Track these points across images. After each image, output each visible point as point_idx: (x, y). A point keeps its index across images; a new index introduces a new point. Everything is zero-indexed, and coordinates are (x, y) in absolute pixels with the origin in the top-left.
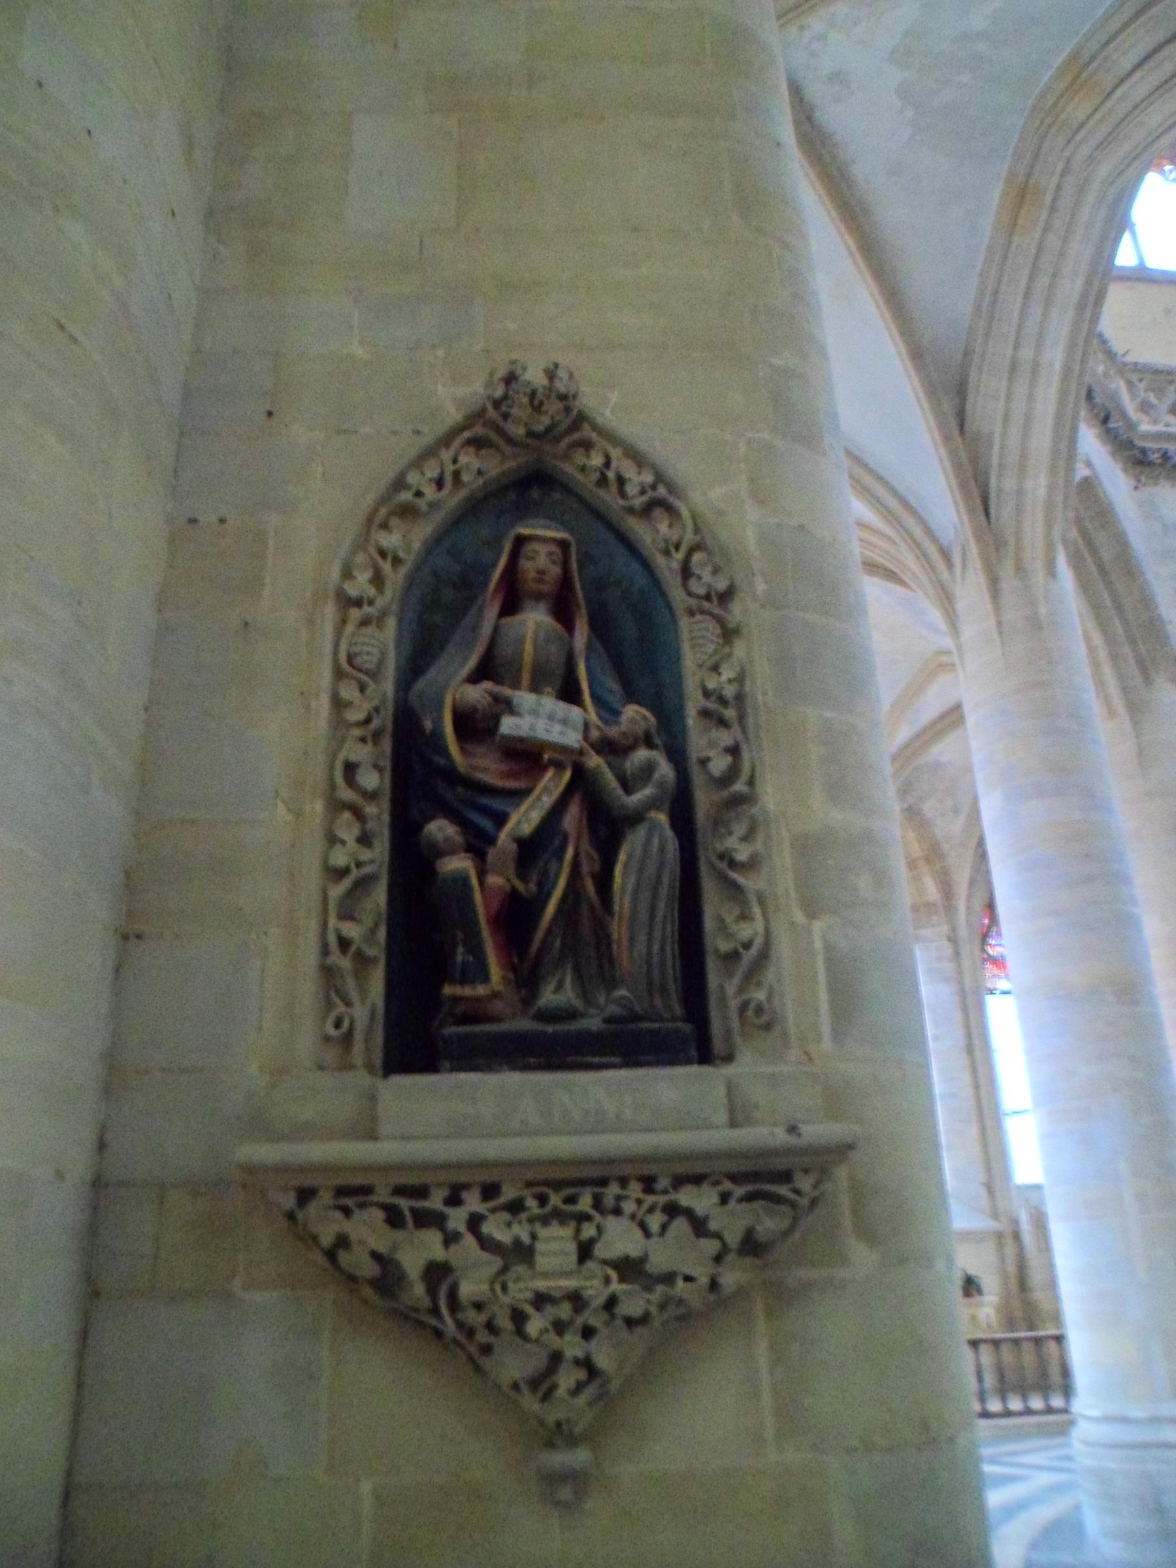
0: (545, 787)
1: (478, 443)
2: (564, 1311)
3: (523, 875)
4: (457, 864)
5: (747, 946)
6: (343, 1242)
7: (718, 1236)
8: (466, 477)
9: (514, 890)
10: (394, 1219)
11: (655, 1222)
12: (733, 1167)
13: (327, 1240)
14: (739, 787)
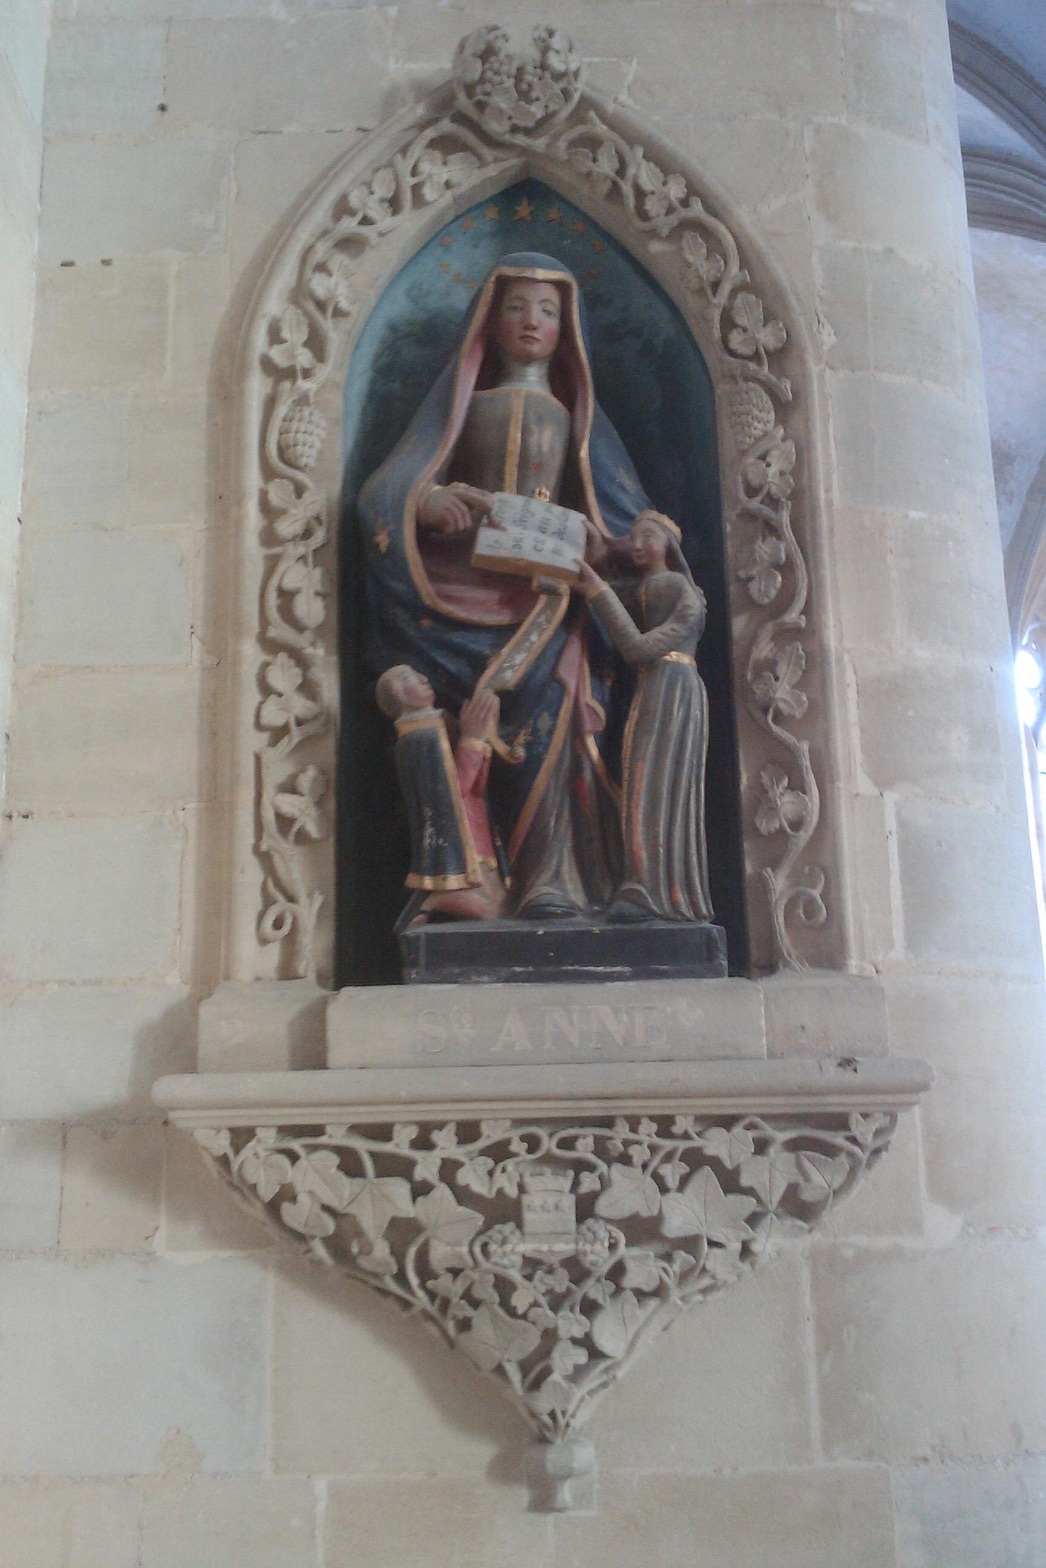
0: (534, 622)
1: (445, 145)
2: (561, 1282)
3: (508, 739)
4: (425, 719)
5: (797, 825)
6: (287, 1194)
7: (750, 1192)
8: (428, 193)
9: (495, 753)
10: (350, 1164)
11: (672, 1173)
12: (779, 1105)
13: (267, 1192)
14: (793, 616)
